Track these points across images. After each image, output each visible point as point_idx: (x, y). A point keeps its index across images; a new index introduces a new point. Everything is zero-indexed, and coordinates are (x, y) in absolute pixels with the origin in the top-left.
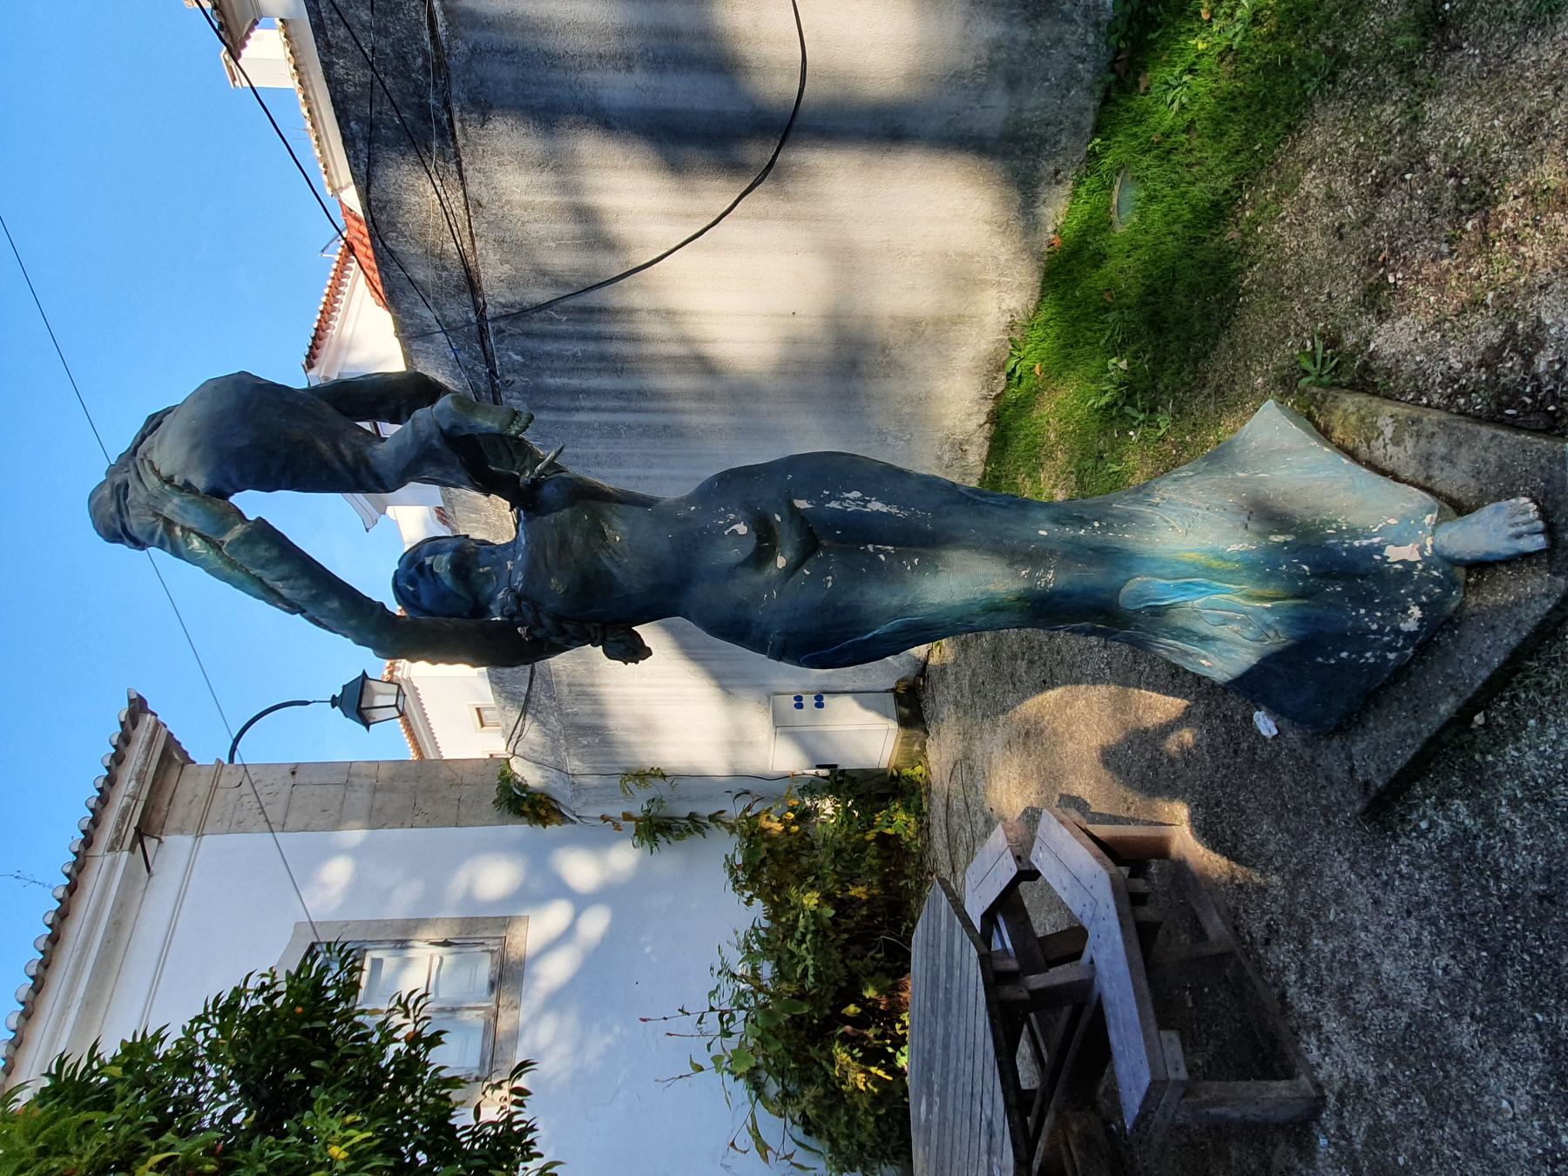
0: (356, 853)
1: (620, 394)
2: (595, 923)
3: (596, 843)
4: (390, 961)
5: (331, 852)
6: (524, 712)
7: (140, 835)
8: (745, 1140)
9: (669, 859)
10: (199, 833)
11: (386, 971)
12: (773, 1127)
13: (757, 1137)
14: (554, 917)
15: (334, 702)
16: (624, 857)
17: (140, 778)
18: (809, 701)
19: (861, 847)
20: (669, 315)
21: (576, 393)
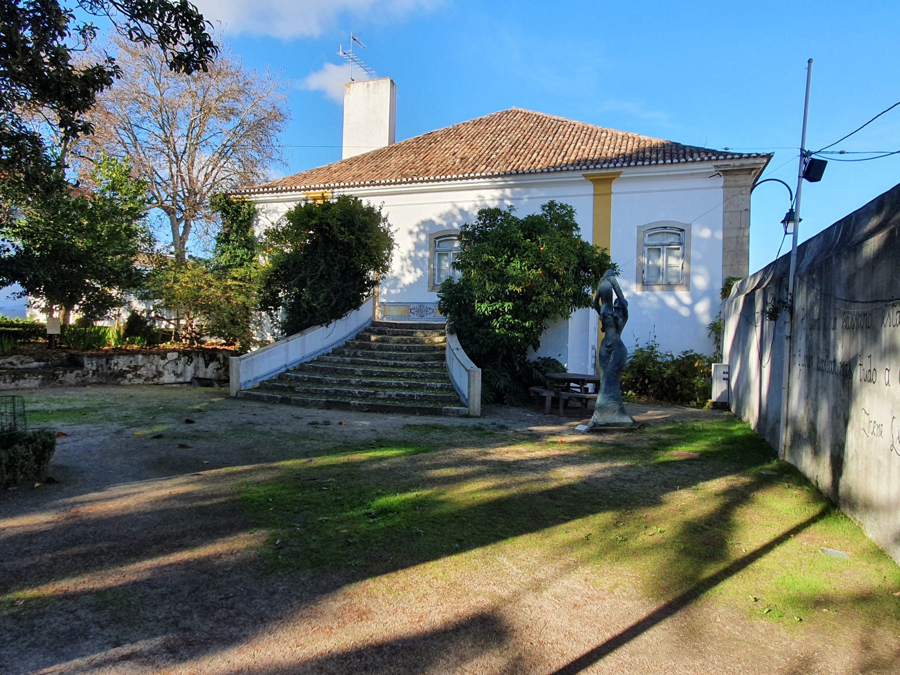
2: (684, 312)
3: (711, 310)
5: (713, 230)
9: (705, 332)
10: (724, 187)
11: (676, 252)
14: (687, 300)
16: (706, 320)
17: (741, 166)
18: (726, 376)
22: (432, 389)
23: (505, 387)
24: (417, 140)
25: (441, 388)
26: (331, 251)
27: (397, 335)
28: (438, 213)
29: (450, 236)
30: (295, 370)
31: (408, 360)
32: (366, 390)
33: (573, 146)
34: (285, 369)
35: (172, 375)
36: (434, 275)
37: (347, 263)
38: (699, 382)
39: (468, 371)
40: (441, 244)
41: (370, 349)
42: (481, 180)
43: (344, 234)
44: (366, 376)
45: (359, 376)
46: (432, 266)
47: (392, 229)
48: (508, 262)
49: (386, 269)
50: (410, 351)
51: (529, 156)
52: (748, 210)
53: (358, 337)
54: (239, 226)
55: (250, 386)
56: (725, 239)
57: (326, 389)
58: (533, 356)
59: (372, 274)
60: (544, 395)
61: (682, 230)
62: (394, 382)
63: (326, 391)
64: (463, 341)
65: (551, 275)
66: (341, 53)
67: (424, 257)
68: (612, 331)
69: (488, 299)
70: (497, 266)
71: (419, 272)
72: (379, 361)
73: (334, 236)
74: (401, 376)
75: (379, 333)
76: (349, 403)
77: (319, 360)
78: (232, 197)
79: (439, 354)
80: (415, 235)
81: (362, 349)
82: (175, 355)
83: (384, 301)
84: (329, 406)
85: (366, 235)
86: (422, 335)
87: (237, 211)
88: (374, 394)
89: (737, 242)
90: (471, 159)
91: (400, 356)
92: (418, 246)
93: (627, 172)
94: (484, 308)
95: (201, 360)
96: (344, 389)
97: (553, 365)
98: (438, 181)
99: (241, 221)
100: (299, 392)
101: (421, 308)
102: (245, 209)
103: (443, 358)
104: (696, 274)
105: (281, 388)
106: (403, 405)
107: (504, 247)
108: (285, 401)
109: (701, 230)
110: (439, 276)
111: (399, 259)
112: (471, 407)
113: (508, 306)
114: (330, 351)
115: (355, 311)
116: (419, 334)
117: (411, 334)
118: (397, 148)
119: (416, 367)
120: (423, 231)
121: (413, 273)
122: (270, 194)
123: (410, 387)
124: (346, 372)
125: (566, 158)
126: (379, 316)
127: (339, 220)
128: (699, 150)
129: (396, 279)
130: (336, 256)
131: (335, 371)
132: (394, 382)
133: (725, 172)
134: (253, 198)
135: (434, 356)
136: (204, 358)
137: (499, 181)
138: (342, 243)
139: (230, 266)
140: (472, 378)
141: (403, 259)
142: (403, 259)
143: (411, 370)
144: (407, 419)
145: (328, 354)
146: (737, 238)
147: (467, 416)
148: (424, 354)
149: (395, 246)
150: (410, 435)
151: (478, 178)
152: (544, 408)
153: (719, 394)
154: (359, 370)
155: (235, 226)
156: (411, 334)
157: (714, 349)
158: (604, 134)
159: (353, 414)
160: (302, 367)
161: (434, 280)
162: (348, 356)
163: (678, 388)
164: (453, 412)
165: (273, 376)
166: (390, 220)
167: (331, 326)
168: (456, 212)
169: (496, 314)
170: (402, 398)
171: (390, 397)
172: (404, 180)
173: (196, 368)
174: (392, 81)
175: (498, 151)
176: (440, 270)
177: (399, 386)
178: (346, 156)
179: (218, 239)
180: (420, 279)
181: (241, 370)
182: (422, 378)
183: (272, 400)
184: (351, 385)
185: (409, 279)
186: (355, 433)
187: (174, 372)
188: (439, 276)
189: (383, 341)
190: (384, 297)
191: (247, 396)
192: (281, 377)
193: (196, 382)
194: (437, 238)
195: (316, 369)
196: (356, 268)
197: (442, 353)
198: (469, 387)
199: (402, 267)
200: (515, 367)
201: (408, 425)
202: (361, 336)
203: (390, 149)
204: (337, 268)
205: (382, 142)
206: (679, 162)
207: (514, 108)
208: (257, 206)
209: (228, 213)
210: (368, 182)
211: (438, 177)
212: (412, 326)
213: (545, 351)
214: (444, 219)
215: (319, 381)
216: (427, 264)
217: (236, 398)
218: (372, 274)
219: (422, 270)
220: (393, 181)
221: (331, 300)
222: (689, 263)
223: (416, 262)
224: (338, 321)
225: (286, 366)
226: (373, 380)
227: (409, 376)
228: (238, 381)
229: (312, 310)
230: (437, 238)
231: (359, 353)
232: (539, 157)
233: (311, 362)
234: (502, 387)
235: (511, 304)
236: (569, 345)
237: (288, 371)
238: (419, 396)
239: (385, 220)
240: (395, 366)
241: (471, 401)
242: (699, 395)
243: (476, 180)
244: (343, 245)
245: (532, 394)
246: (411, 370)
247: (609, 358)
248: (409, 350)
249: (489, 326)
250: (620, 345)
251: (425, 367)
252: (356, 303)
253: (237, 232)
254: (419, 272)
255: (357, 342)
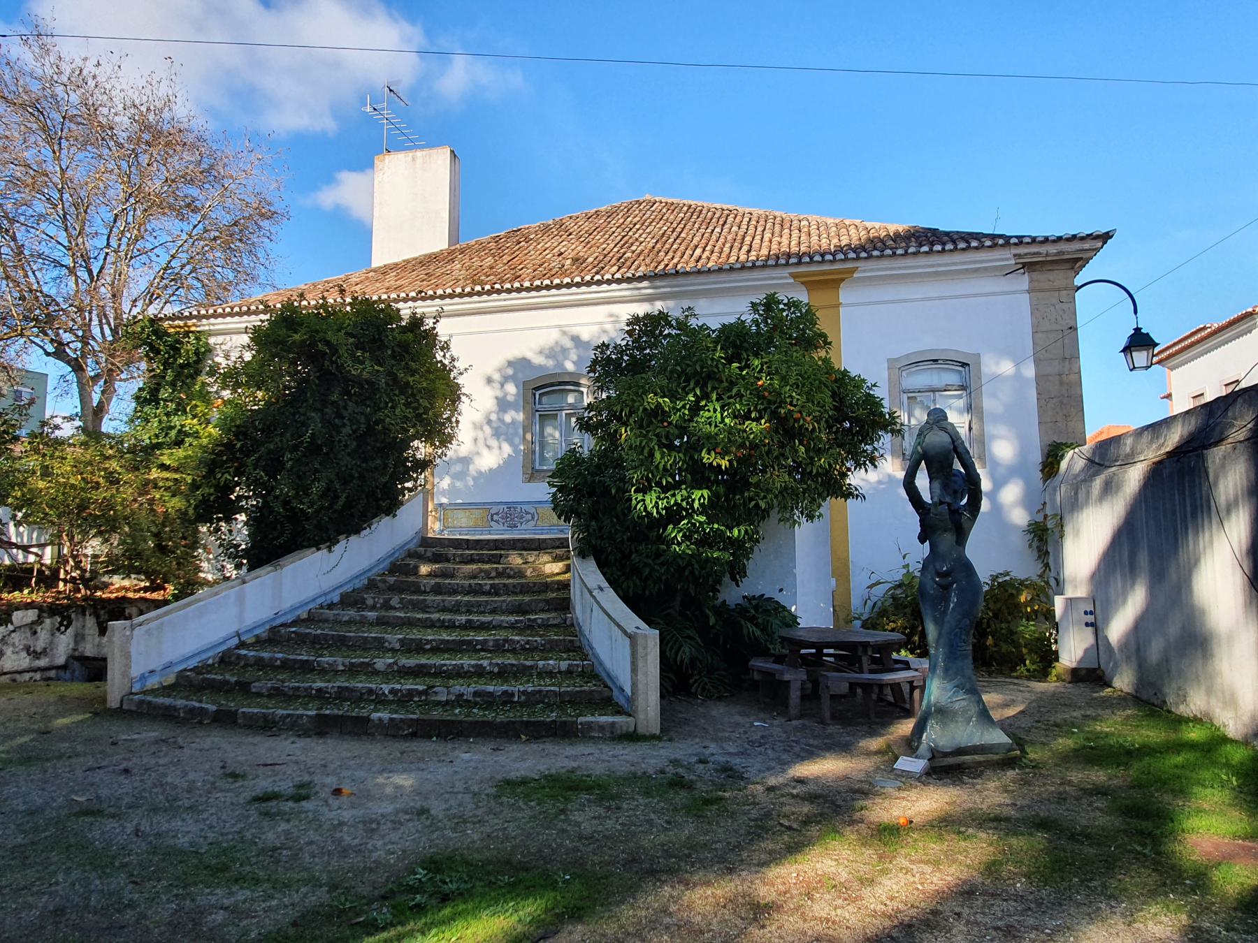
0: (1018, 376)
1: (1185, 516)
3: (1026, 502)
4: (961, 403)
6: (1088, 459)
7: (1024, 265)
8: (874, 579)
9: (1019, 542)
12: (880, 591)
13: (878, 583)
15: (1138, 330)
16: (1020, 517)
18: (1090, 618)
19: (1018, 646)
20: (1211, 542)
21: (1184, 493)
22: (551, 674)
23: (693, 660)
24: (497, 240)
25: (569, 673)
26: (335, 397)
27: (471, 561)
28: (536, 347)
29: (560, 383)
30: (259, 642)
31: (493, 612)
32: (409, 685)
33: (758, 238)
34: (235, 641)
35: (24, 654)
36: (533, 452)
37: (368, 420)
38: (1028, 629)
39: (630, 636)
40: (544, 399)
41: (418, 591)
42: (614, 286)
43: (362, 363)
44: (409, 651)
45: (393, 650)
46: (529, 437)
47: (460, 365)
48: (696, 409)
49: (446, 440)
50: (497, 594)
51: (689, 252)
52: (1073, 329)
53: (395, 568)
54: (178, 376)
55: (153, 682)
56: (1040, 378)
57: (319, 684)
58: (731, 594)
59: (422, 449)
60: (787, 677)
61: (964, 365)
62: (467, 662)
63: (319, 690)
64: (605, 570)
65: (787, 430)
66: (369, 109)
67: (514, 422)
68: (948, 539)
69: (659, 484)
70: (674, 418)
71: (507, 449)
72: (435, 616)
73: (340, 368)
74: (484, 647)
75: (436, 559)
76: (367, 720)
77: (311, 619)
78: (166, 324)
79: (558, 597)
80: (497, 385)
81: (401, 591)
82: (31, 615)
83: (444, 500)
84: (322, 727)
85: (407, 367)
86: (519, 561)
87: (175, 348)
88: (425, 692)
89: (1061, 383)
90: (590, 260)
91: (479, 604)
92: (503, 405)
93: (867, 269)
94: (651, 502)
95: (90, 622)
96: (360, 684)
97: (769, 611)
98: (538, 288)
99: (182, 366)
100: (259, 695)
101: (511, 513)
102: (189, 345)
103: (564, 605)
104: (994, 437)
105: (222, 691)
106: (490, 716)
107: (688, 381)
108: (225, 720)
109: (997, 363)
110: (542, 454)
111: (470, 426)
112: (641, 716)
113: (700, 496)
114: (336, 599)
115: (386, 520)
116: (515, 560)
117: (497, 559)
118: (462, 252)
119: (512, 627)
120: (513, 378)
121: (496, 451)
122: (237, 319)
123: (504, 674)
124: (364, 645)
125: (753, 253)
126: (435, 528)
127: (351, 335)
128: (967, 237)
129: (466, 461)
130: (345, 408)
131: (341, 643)
132: (467, 662)
133: (1029, 267)
134: (205, 325)
135: (547, 602)
136: (98, 617)
137: (645, 288)
138: (358, 382)
139: (159, 446)
140: (640, 650)
141: (477, 427)
142: (477, 427)
143: (501, 635)
144: (502, 758)
145: (331, 606)
146: (1060, 375)
147: (633, 737)
148: (527, 599)
149: (463, 398)
150: (515, 826)
151: (609, 282)
152: (785, 704)
153: (1079, 653)
154: (394, 638)
155: (170, 375)
156: (497, 559)
157: (1039, 568)
158: (804, 223)
159: (376, 750)
160: (274, 636)
161: (533, 462)
162: (373, 608)
163: (990, 641)
164: (601, 728)
165: (210, 657)
166: (455, 350)
167: (338, 548)
168: (568, 344)
169: (673, 515)
170: (488, 701)
171: (460, 701)
172: (478, 288)
173: (79, 638)
174: (452, 152)
175: (634, 248)
176: (543, 445)
177: (479, 673)
178: (377, 263)
179: (137, 398)
180: (508, 462)
181: (133, 650)
182: (528, 650)
183: (194, 719)
184: (377, 673)
185: (489, 460)
186: (371, 826)
187: (27, 649)
188: (542, 454)
189: (444, 574)
190: (443, 493)
191: (142, 709)
192: (226, 660)
193: (76, 664)
194: (537, 389)
195: (302, 640)
196: (386, 430)
197: (561, 595)
198: (634, 669)
199: (476, 440)
200: (707, 617)
201: (508, 782)
202: (400, 569)
203: (451, 253)
204: (347, 430)
205: (438, 242)
206: (956, 248)
207: (648, 197)
208: (212, 341)
209: (158, 352)
210: (413, 294)
211: (537, 283)
212: (498, 545)
213: (757, 583)
214: (548, 357)
215: (307, 668)
216: (521, 431)
217: (120, 713)
218: (422, 449)
219: (511, 444)
220: (458, 290)
221: (337, 497)
222: (981, 419)
223: (500, 432)
224: (353, 538)
225: (238, 634)
226: (423, 661)
227: (499, 648)
228: (125, 674)
229: (295, 517)
230: (537, 389)
231: (395, 601)
232: (707, 253)
233: (294, 623)
234: (687, 661)
235: (706, 493)
236: (797, 571)
237: (242, 645)
238: (524, 693)
239: (446, 347)
240: (469, 626)
241: (640, 701)
242: (1031, 651)
243: (605, 287)
244: (361, 387)
245: (756, 676)
246: (501, 635)
247: (946, 600)
248: (495, 590)
249: (661, 539)
250: (968, 568)
251: (530, 627)
252: (388, 503)
253: (173, 384)
254: (507, 449)
255: (391, 580)
